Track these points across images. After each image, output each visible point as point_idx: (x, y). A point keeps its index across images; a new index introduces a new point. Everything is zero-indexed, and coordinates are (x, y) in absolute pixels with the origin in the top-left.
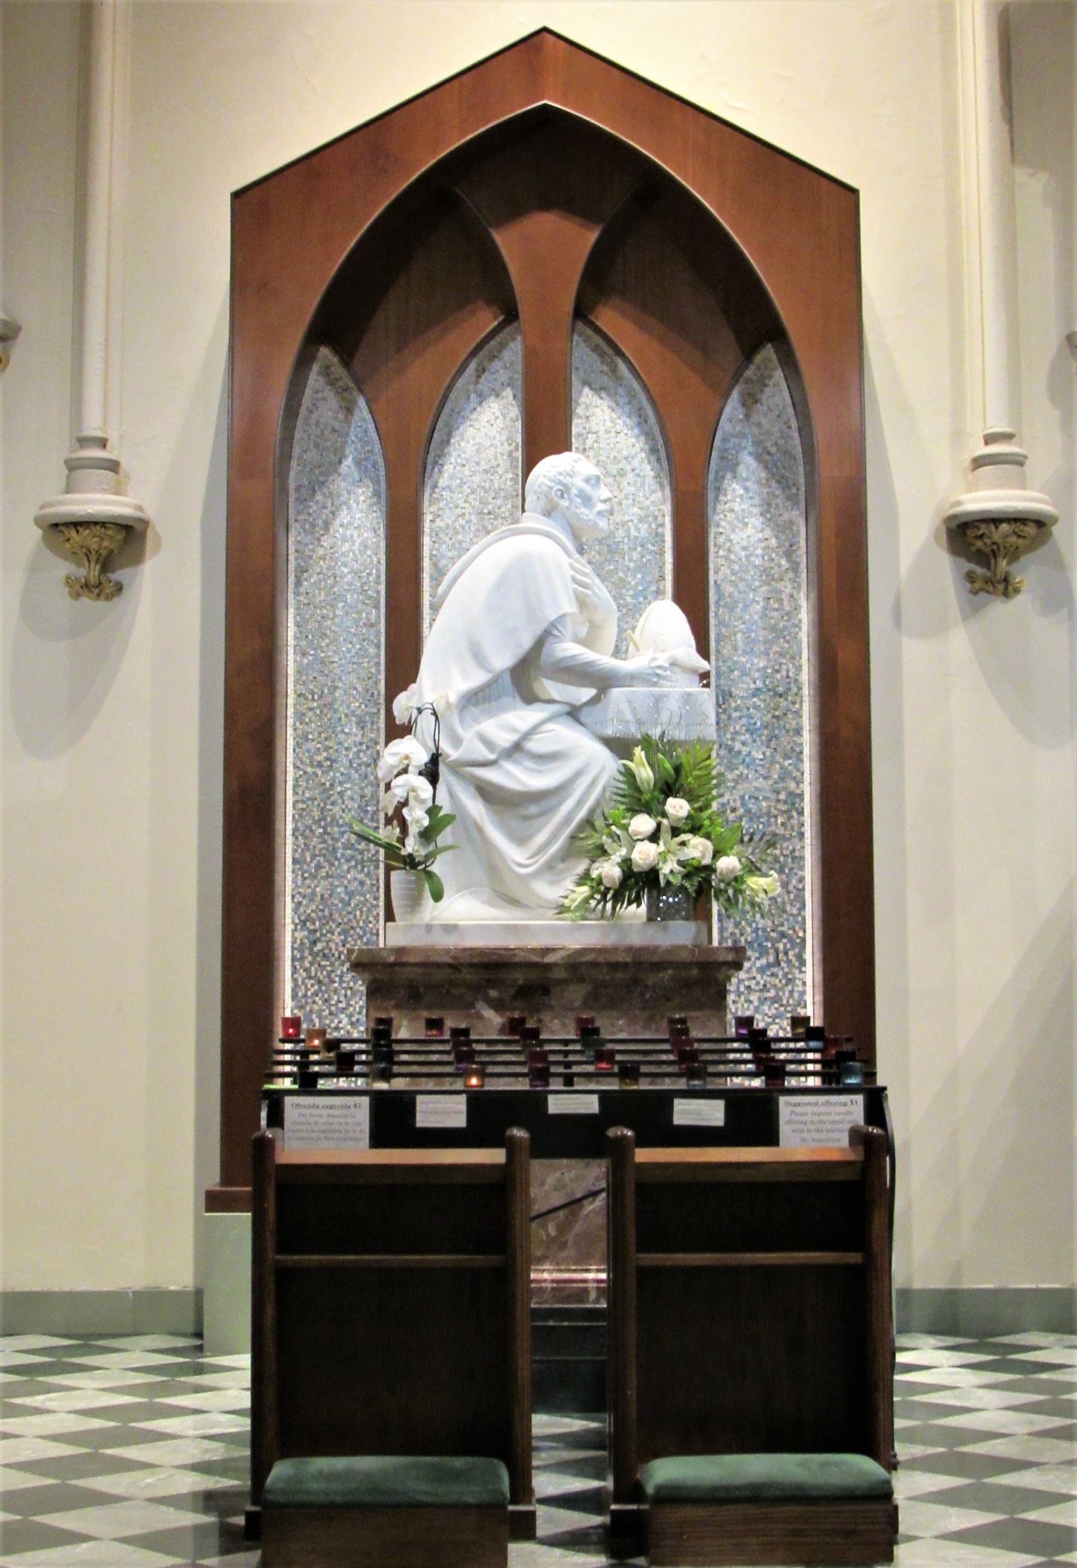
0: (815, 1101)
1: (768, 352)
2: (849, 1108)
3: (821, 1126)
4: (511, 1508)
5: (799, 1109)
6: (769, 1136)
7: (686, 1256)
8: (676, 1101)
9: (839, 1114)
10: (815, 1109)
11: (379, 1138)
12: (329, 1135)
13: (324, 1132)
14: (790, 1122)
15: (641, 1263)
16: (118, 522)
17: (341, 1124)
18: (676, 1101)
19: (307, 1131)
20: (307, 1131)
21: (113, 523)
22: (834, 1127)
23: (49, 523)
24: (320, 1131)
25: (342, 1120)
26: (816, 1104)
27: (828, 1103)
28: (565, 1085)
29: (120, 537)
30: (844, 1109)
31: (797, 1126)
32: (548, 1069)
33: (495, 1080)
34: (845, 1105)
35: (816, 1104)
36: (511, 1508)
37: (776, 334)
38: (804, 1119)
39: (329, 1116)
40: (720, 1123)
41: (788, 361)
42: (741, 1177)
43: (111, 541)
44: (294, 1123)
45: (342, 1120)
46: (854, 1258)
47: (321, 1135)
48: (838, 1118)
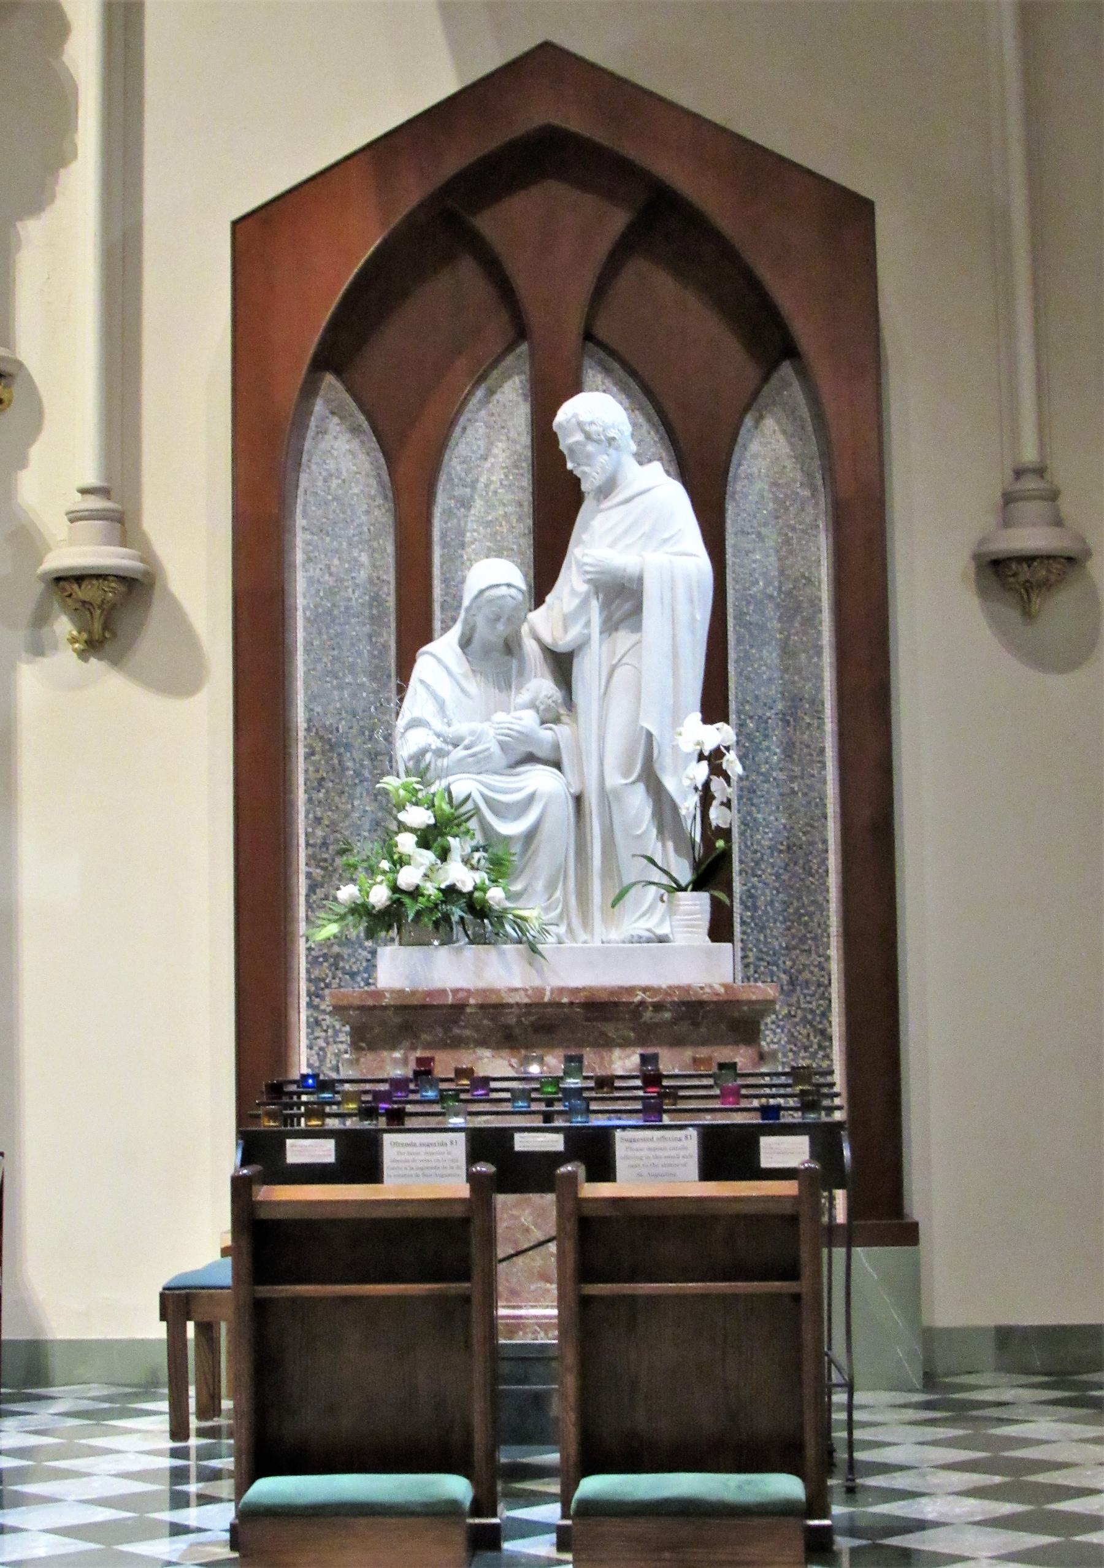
0: (650, 1137)
1: (786, 369)
2: (684, 1143)
3: (656, 1162)
4: (470, 1521)
5: (635, 1145)
6: (372, 1172)
7: (319, 1287)
8: (289, 1142)
9: (674, 1149)
10: (651, 1145)
11: (708, 1172)
12: (427, 1172)
13: (422, 1169)
14: (626, 1158)
15: (259, 1295)
16: (121, 574)
17: (438, 1160)
18: (289, 1142)
19: (406, 1168)
20: (406, 1168)
21: (115, 576)
22: (669, 1161)
23: (988, 559)
24: (418, 1169)
25: (438, 1157)
26: (652, 1140)
27: (663, 1138)
28: (545, 1122)
29: (122, 588)
30: (679, 1144)
31: (632, 1162)
32: (819, 1101)
33: (414, 1119)
34: (680, 1140)
35: (652, 1140)
36: (470, 1521)
37: (789, 351)
38: (638, 1154)
39: (427, 1153)
40: (331, 1158)
41: (804, 374)
42: (328, 1213)
43: (111, 592)
44: (394, 1161)
45: (438, 1157)
46: (266, 1291)
47: (420, 1172)
48: (673, 1153)
